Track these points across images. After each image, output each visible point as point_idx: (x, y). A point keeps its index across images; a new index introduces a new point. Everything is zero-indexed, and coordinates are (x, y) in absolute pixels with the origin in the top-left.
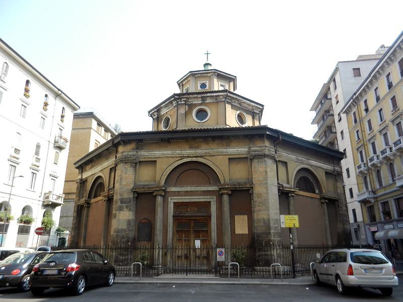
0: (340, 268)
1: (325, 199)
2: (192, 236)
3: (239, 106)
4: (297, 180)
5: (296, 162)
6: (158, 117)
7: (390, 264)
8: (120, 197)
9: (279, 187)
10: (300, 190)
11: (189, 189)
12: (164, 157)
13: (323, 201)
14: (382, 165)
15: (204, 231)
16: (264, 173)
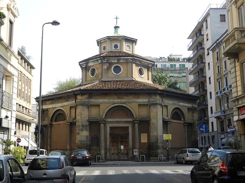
0: (184, 155)
1: (187, 123)
2: (119, 144)
3: (140, 64)
4: (172, 114)
5: (172, 104)
6: (86, 67)
7: (201, 153)
8: (81, 124)
9: (163, 120)
10: (173, 119)
11: (117, 120)
12: (104, 103)
13: (185, 124)
14: (230, 94)
15: (125, 141)
16: (156, 113)
